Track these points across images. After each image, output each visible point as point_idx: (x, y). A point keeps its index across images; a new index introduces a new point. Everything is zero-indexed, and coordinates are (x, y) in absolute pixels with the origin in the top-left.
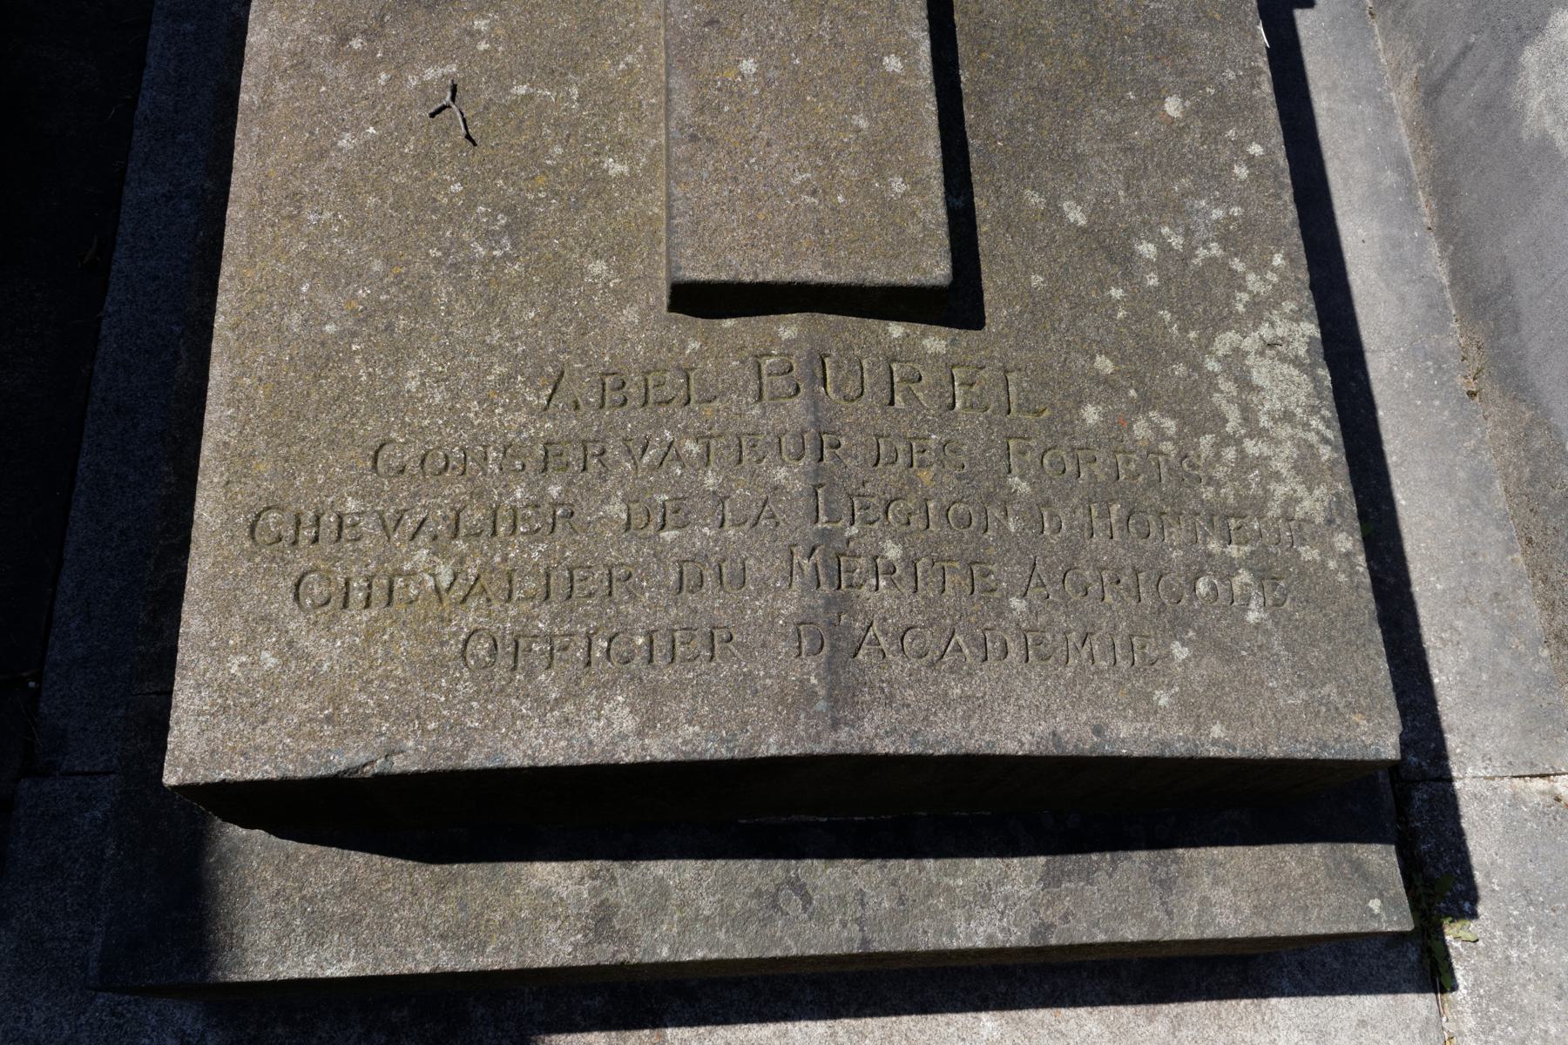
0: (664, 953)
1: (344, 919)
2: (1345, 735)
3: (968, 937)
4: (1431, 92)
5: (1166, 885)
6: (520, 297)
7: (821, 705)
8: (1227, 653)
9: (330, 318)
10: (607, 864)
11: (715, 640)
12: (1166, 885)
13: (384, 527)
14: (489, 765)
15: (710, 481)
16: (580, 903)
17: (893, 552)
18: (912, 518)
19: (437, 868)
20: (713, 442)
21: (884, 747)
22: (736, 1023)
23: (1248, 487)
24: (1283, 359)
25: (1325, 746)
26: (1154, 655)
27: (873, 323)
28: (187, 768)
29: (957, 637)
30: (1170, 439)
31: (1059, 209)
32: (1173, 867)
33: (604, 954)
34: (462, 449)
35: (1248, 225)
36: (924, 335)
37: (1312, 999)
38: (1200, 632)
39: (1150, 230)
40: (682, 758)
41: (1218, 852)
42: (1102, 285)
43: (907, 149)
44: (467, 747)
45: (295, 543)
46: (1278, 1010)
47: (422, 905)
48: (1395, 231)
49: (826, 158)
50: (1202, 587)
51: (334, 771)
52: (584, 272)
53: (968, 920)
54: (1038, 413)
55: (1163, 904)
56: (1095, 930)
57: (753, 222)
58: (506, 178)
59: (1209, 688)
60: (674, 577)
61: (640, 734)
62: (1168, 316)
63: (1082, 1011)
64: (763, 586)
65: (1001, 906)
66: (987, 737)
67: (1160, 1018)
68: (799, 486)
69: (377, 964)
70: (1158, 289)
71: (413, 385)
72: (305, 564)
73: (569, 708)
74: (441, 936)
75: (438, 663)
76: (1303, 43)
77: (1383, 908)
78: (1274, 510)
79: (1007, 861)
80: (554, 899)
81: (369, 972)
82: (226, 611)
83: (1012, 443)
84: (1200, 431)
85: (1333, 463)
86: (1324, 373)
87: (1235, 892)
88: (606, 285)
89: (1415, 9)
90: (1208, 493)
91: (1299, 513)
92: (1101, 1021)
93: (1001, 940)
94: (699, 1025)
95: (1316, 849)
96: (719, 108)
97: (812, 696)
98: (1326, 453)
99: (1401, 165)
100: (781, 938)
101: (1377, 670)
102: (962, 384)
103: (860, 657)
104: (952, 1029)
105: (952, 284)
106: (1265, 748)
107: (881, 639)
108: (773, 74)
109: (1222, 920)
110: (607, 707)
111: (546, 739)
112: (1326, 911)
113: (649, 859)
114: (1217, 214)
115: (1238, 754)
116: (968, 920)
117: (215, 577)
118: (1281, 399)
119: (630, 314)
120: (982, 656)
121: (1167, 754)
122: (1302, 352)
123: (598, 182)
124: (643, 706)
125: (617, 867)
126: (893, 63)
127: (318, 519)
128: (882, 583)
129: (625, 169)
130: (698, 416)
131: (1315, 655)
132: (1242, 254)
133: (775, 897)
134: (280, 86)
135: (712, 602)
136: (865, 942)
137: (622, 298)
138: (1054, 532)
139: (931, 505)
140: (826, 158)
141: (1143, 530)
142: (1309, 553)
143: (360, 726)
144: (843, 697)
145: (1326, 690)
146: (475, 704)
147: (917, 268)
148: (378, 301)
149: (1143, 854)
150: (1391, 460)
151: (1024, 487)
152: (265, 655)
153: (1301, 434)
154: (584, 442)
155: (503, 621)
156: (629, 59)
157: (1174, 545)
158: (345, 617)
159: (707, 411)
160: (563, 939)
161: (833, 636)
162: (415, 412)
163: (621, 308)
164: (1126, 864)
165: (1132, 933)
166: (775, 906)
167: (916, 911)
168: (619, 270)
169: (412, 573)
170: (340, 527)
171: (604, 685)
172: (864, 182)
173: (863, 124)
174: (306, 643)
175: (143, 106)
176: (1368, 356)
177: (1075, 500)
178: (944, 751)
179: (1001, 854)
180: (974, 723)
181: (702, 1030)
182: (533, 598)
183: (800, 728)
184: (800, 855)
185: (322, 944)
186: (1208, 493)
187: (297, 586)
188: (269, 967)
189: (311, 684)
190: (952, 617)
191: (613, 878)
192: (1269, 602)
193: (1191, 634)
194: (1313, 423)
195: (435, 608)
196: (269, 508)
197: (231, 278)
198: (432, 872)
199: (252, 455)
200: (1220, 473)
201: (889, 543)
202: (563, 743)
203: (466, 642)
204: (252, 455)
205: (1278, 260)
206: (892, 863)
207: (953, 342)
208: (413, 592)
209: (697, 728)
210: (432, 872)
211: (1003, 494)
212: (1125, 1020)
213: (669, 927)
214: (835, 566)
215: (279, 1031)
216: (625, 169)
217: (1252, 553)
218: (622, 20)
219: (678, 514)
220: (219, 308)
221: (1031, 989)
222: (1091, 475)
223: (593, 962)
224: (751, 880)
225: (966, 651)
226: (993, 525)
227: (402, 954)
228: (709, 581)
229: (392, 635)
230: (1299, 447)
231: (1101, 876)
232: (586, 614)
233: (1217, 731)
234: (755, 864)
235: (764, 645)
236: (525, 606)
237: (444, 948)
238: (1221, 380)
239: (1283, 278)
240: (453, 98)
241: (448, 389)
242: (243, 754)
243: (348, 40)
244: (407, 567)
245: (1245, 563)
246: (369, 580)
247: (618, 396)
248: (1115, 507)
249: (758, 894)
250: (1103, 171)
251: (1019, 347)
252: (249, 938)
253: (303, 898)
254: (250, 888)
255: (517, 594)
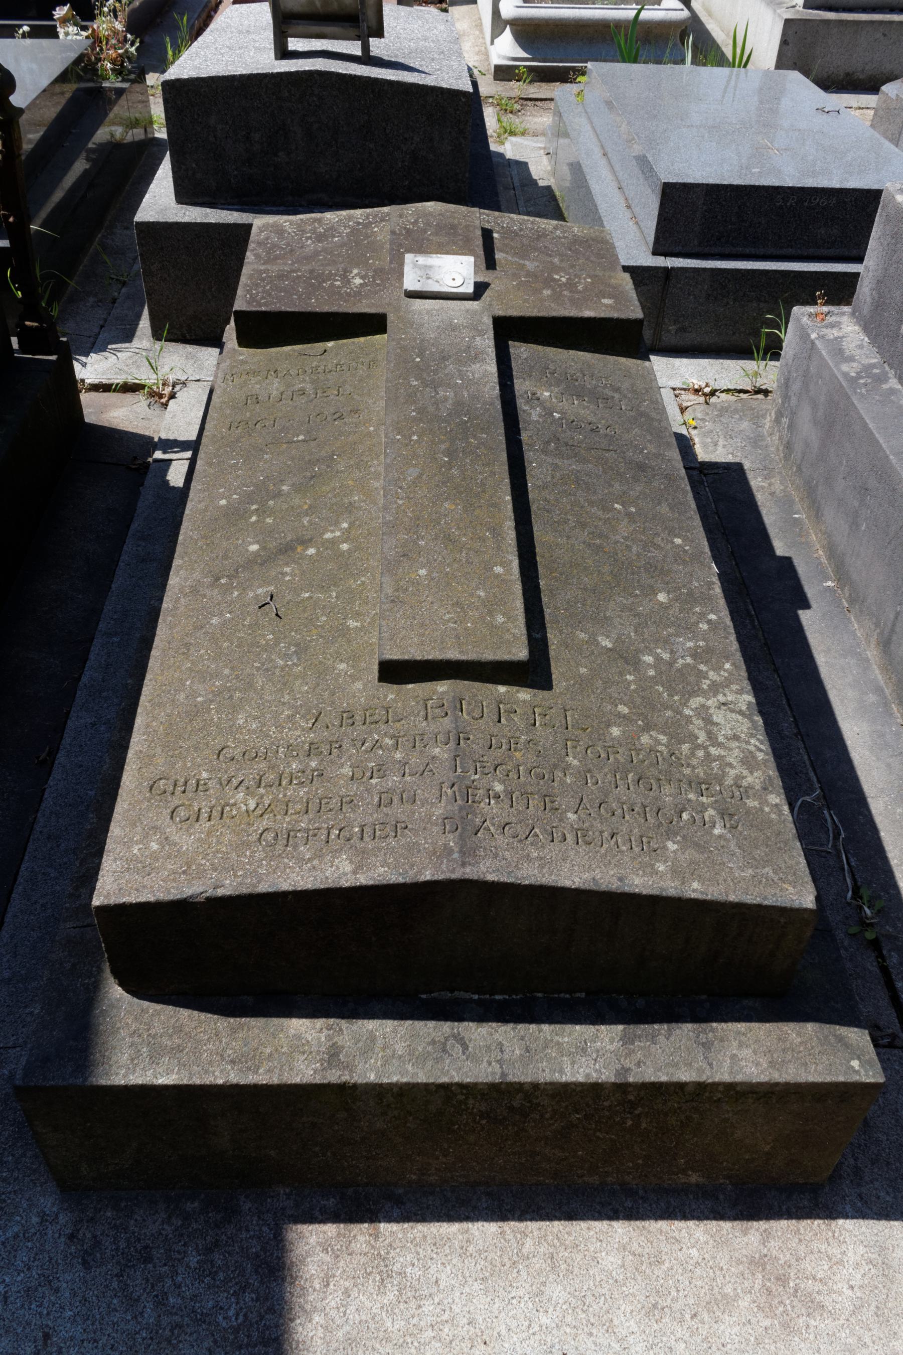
0: (372, 1077)
1: (173, 1049)
2: (779, 894)
3: (573, 1075)
4: (886, 645)
5: (707, 1046)
6: (300, 681)
7: (456, 855)
8: (700, 847)
9: (200, 695)
10: (338, 1021)
11: (399, 828)
12: (707, 1046)
13: (221, 785)
14: (270, 890)
15: (398, 756)
16: (320, 1044)
17: (499, 787)
18: (510, 774)
19: (232, 1020)
20: (400, 739)
21: (490, 877)
22: (431, 1221)
23: (712, 769)
24: (732, 711)
25: (765, 898)
26: (656, 846)
27: (490, 686)
28: (106, 897)
29: (536, 830)
30: (664, 745)
31: (596, 640)
32: (710, 1035)
33: (334, 1076)
34: (265, 748)
35: (709, 650)
36: (518, 692)
37: (871, 1222)
38: (684, 837)
39: (650, 650)
40: (377, 883)
41: (741, 1026)
42: (621, 674)
43: (505, 603)
44: (259, 882)
45: (173, 793)
46: (845, 1229)
47: (221, 1042)
48: (879, 727)
49: (462, 608)
50: (685, 816)
51: (185, 896)
52: (334, 668)
53: (573, 1063)
54: (584, 730)
55: (705, 1058)
56: (660, 1074)
57: (423, 635)
58: (296, 631)
59: (690, 865)
60: (376, 800)
61: (355, 873)
62: (661, 689)
63: (691, 1224)
64: (425, 802)
65: (594, 1055)
66: (553, 877)
67: (752, 1231)
68: (446, 756)
69: (191, 1076)
70: (655, 677)
71: (241, 722)
72: (177, 802)
73: (316, 862)
74: (231, 1061)
75: (248, 845)
76: (806, 628)
77: (861, 1065)
78: (729, 781)
79: (597, 1027)
80: (303, 1041)
81: (185, 1082)
82: (134, 825)
83: (569, 743)
84: (681, 742)
85: (765, 762)
86: (759, 719)
87: (755, 1052)
88: (346, 673)
89: (869, 601)
90: (687, 771)
91: (745, 783)
92: (706, 1232)
93: (594, 1077)
94: (404, 1222)
95: (810, 1027)
96: (407, 589)
97: (451, 851)
98: (760, 756)
99: (879, 690)
100: (448, 1071)
101: (798, 863)
102: (539, 715)
103: (479, 835)
104: (592, 1233)
105: (528, 660)
106: (727, 896)
107: (491, 828)
108: (435, 575)
109: (748, 1071)
110: (336, 861)
111: (302, 877)
112: (820, 1068)
113: (364, 1019)
114: (690, 644)
115: (709, 897)
116: (573, 1063)
117: (130, 810)
118: (731, 729)
119: (359, 685)
120: (550, 839)
121: (664, 894)
122: (744, 708)
123: (344, 631)
124: (357, 860)
125: (344, 1023)
126: (498, 569)
127: (186, 783)
128: (492, 802)
129: (359, 624)
130: (392, 728)
131: (757, 853)
132: (706, 663)
133: (445, 1044)
134: (183, 600)
135: (398, 811)
136: (503, 1074)
137: (354, 678)
138: (593, 784)
139: (521, 768)
140: (462, 608)
141: (649, 787)
142: (752, 803)
143: (201, 873)
144: (468, 853)
145: (767, 870)
146: (264, 862)
147: (510, 653)
148: (225, 686)
149: (689, 1026)
150: (894, 862)
151: (576, 762)
152: (153, 844)
153: (744, 746)
154: (331, 742)
155: (282, 824)
156: (363, 579)
157: (667, 795)
158: (197, 826)
159: (398, 725)
160: (307, 1066)
161: (465, 826)
162: (241, 733)
163: (353, 682)
164: (678, 1032)
165: (685, 1076)
166: (444, 1050)
167: (537, 1057)
168: (353, 666)
169: (235, 804)
170: (198, 785)
171: (336, 851)
172: (482, 618)
173: (482, 594)
174: (175, 838)
175: (85, 679)
176: (869, 800)
177: (606, 770)
178: (527, 882)
179: (593, 1023)
180: (545, 870)
181: (406, 1225)
182: (299, 813)
183: (444, 866)
184: (460, 1019)
185: (158, 1064)
186: (687, 771)
187: (173, 813)
188: (124, 1076)
189: (176, 857)
190: (533, 820)
191: (341, 1029)
192: (728, 826)
193: (679, 838)
194: (752, 741)
195: (246, 820)
196: (161, 779)
197: (151, 680)
198: (229, 1022)
199: (154, 756)
200: (694, 762)
201: (496, 784)
202: (312, 879)
203: (261, 834)
204: (154, 756)
205: (727, 666)
206: (520, 1026)
207: (535, 695)
208: (234, 812)
209: (386, 869)
210: (229, 1022)
211: (563, 765)
212: (725, 1232)
213: (375, 1061)
214: (467, 794)
215: (109, 1214)
216: (359, 624)
217: (716, 801)
218: (360, 564)
219: (381, 770)
220: (143, 693)
221: (651, 1205)
222: (616, 759)
223: (326, 1081)
224: (429, 1034)
225: (541, 837)
226: (557, 779)
227: (207, 1072)
228: (396, 800)
229: (221, 833)
230: (743, 752)
231: (661, 1038)
232: (328, 819)
233: (695, 885)
234: (431, 1024)
235: (425, 829)
236: (294, 817)
237: (233, 1069)
238: (694, 719)
239: (731, 674)
240: (271, 600)
241: (260, 722)
242: (137, 890)
243: (219, 579)
244: (232, 801)
245: (711, 805)
246: (212, 808)
247: (350, 721)
248: (630, 776)
249: (433, 1042)
250: (621, 624)
251: (572, 699)
252: (114, 1059)
253: (149, 1035)
254: (118, 1028)
255: (290, 812)
